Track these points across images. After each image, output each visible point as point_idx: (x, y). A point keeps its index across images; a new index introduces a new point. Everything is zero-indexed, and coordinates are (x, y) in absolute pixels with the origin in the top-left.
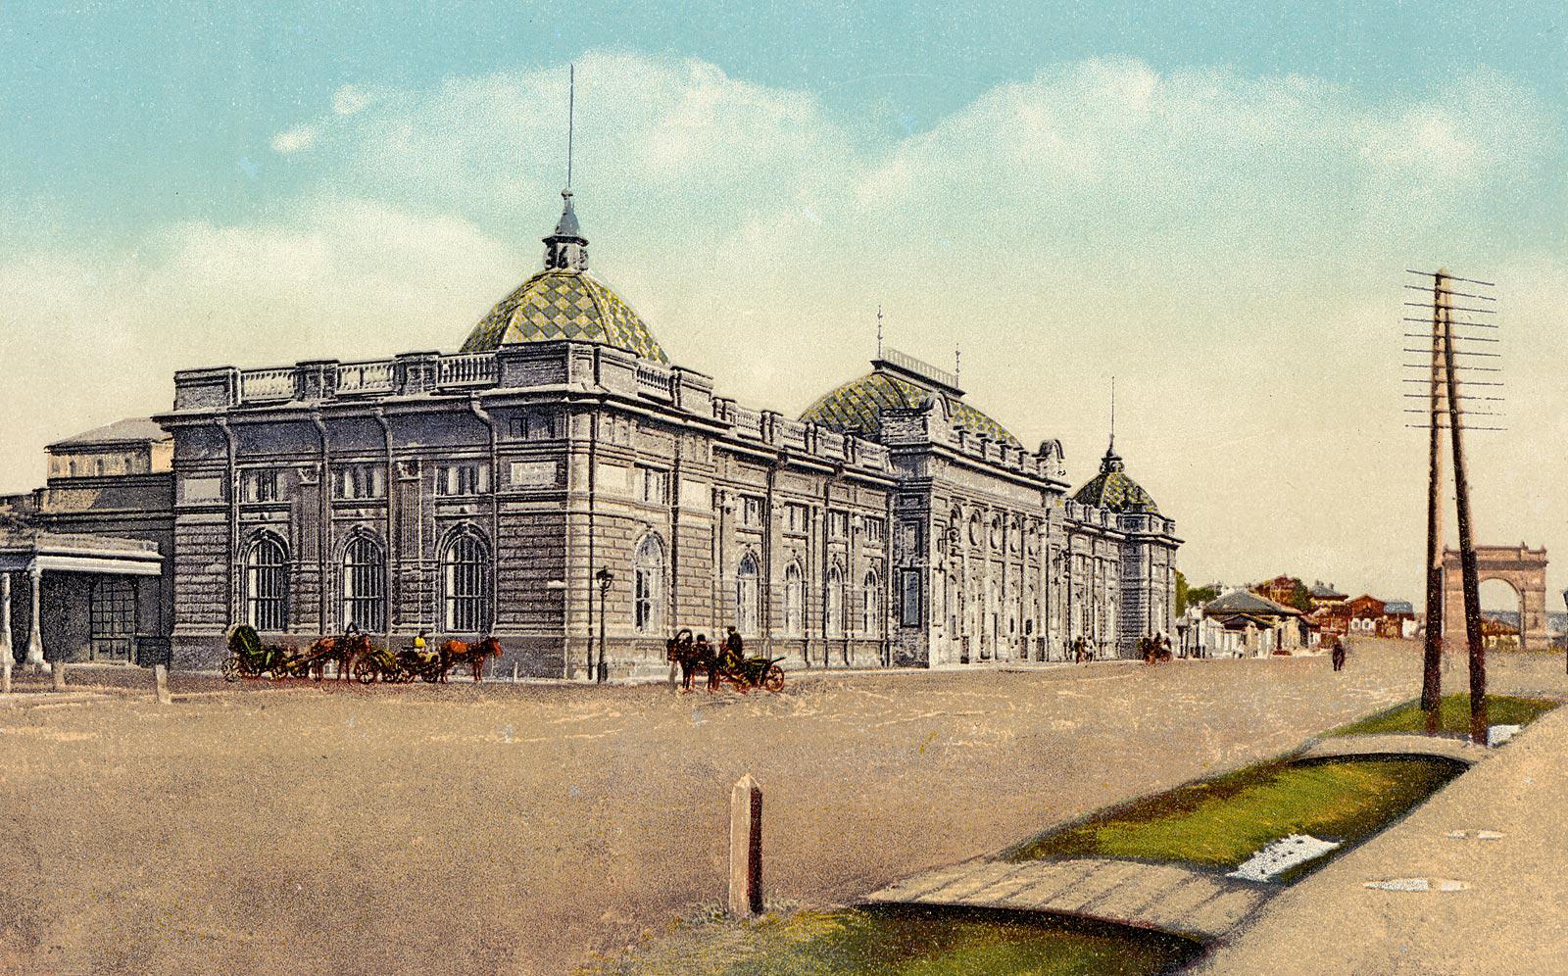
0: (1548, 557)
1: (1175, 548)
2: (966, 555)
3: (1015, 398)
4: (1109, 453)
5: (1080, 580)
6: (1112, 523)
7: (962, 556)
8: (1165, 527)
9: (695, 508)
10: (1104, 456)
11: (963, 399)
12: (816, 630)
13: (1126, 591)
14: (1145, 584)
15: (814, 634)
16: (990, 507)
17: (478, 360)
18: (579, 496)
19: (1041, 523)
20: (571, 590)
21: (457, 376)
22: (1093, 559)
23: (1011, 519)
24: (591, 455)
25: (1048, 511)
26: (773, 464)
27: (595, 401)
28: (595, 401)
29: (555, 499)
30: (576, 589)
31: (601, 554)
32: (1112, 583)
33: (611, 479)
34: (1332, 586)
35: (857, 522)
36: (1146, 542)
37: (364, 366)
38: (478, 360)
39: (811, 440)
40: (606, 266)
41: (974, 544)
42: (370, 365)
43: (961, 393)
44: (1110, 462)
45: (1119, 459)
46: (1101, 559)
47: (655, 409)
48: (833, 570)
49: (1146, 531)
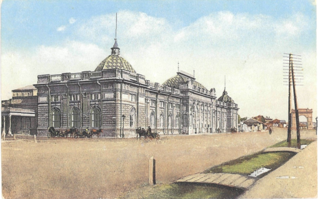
0: (313, 111)
1: (238, 110)
2: (196, 112)
4: (224, 91)
5: (219, 117)
8: (236, 106)
9: (142, 102)
11: (195, 80)
13: (228, 119)
14: (232, 117)
19: (211, 105)
22: (222, 112)
23: (205, 104)
24: (121, 92)
25: (212, 102)
26: (157, 93)
27: (121, 81)
29: (114, 100)
32: (225, 117)
33: (125, 97)
39: (165, 88)
43: (195, 79)
44: (225, 93)
45: (226, 92)
49: (232, 107)
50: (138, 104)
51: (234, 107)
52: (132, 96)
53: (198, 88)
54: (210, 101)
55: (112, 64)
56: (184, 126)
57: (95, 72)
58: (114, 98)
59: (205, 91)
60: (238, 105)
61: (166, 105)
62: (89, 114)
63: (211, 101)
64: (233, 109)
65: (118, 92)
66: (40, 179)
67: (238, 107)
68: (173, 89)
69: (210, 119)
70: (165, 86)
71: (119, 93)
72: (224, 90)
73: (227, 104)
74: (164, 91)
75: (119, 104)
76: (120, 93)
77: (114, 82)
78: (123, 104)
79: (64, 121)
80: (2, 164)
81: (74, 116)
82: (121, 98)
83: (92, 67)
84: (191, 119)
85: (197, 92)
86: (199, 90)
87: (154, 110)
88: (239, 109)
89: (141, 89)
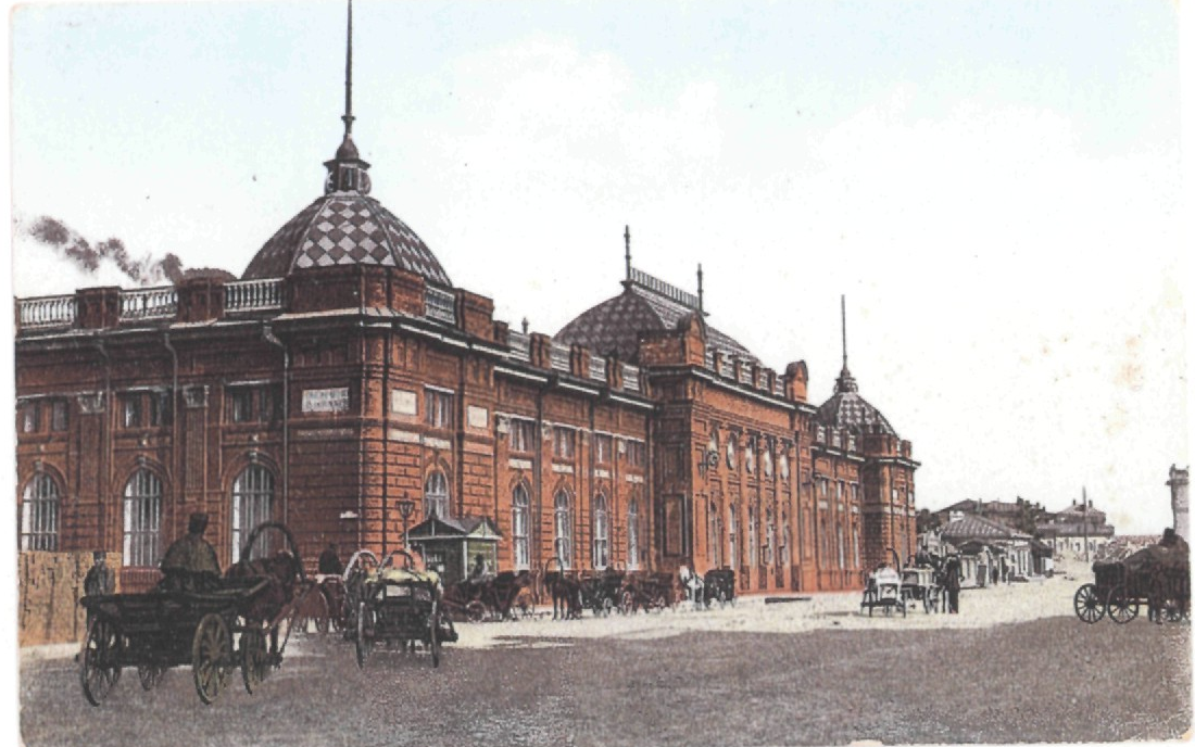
1: (913, 469)
2: (724, 480)
3: (760, 319)
4: (844, 373)
6: (851, 446)
7: (720, 482)
9: (477, 433)
10: (838, 375)
12: (584, 561)
13: (867, 516)
15: (583, 564)
16: (744, 429)
17: (261, 287)
18: (372, 423)
19: (791, 446)
20: (364, 520)
21: (252, 301)
22: (835, 483)
23: (763, 442)
24: (385, 380)
25: (797, 433)
26: (547, 391)
27: (389, 325)
28: (389, 325)
29: (346, 425)
30: (371, 519)
31: (412, 463)
32: (855, 509)
33: (404, 403)
34: (525, 324)
35: (622, 448)
36: (885, 464)
37: (147, 293)
38: (261, 287)
39: (575, 361)
40: (388, 188)
41: (731, 469)
42: (153, 292)
44: (844, 383)
46: (843, 483)
47: (445, 333)
48: (599, 496)
49: (886, 454)
50: (461, 445)
51: (896, 458)
52: (434, 399)
53: (731, 362)
54: (787, 425)
55: (333, 241)
56: (665, 554)
57: (242, 283)
58: (347, 413)
59: (762, 385)
60: (914, 449)
61: (581, 445)
62: (216, 494)
63: (792, 426)
64: (890, 465)
65: (371, 384)
66: (800, 708)
67: (914, 457)
68: (615, 364)
69: (786, 523)
70: (576, 349)
71: (375, 387)
72: (840, 368)
73: (876, 453)
74: (532, 363)
75: (378, 440)
76: (380, 387)
77: (352, 334)
78: (468, 453)
79: (80, 531)
80: (1186, 640)
81: (133, 504)
82: (385, 411)
83: (228, 245)
84: (702, 521)
85: (724, 379)
86: (736, 375)
87: (529, 476)
88: (919, 464)
89: (475, 363)
